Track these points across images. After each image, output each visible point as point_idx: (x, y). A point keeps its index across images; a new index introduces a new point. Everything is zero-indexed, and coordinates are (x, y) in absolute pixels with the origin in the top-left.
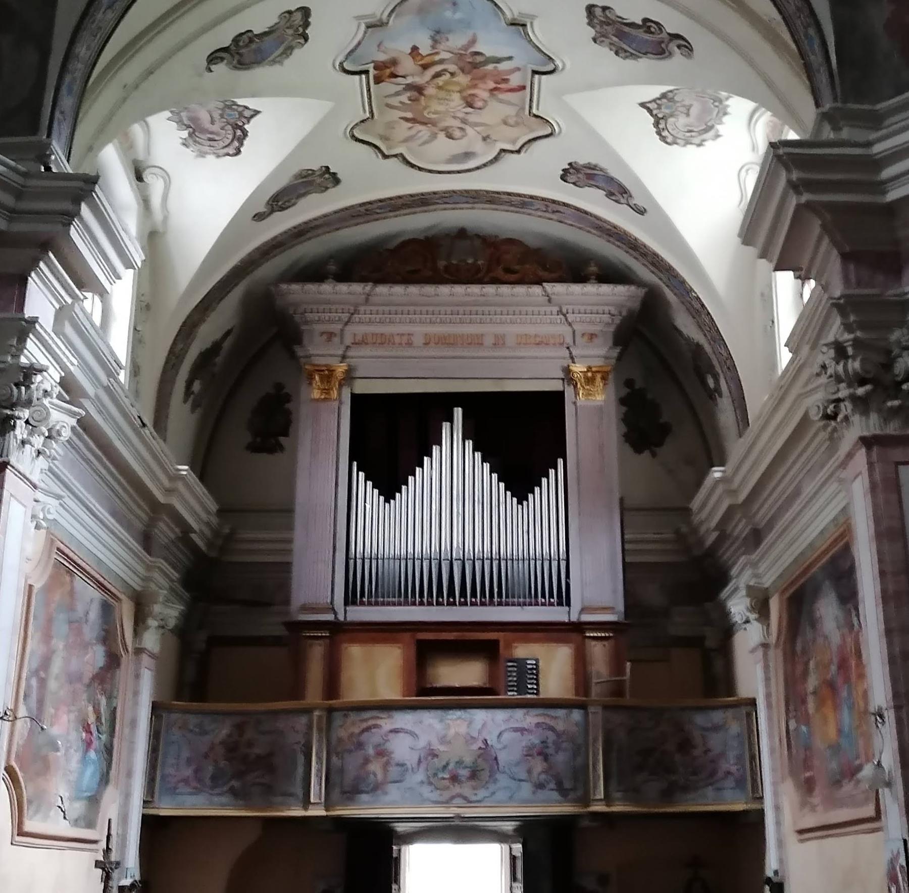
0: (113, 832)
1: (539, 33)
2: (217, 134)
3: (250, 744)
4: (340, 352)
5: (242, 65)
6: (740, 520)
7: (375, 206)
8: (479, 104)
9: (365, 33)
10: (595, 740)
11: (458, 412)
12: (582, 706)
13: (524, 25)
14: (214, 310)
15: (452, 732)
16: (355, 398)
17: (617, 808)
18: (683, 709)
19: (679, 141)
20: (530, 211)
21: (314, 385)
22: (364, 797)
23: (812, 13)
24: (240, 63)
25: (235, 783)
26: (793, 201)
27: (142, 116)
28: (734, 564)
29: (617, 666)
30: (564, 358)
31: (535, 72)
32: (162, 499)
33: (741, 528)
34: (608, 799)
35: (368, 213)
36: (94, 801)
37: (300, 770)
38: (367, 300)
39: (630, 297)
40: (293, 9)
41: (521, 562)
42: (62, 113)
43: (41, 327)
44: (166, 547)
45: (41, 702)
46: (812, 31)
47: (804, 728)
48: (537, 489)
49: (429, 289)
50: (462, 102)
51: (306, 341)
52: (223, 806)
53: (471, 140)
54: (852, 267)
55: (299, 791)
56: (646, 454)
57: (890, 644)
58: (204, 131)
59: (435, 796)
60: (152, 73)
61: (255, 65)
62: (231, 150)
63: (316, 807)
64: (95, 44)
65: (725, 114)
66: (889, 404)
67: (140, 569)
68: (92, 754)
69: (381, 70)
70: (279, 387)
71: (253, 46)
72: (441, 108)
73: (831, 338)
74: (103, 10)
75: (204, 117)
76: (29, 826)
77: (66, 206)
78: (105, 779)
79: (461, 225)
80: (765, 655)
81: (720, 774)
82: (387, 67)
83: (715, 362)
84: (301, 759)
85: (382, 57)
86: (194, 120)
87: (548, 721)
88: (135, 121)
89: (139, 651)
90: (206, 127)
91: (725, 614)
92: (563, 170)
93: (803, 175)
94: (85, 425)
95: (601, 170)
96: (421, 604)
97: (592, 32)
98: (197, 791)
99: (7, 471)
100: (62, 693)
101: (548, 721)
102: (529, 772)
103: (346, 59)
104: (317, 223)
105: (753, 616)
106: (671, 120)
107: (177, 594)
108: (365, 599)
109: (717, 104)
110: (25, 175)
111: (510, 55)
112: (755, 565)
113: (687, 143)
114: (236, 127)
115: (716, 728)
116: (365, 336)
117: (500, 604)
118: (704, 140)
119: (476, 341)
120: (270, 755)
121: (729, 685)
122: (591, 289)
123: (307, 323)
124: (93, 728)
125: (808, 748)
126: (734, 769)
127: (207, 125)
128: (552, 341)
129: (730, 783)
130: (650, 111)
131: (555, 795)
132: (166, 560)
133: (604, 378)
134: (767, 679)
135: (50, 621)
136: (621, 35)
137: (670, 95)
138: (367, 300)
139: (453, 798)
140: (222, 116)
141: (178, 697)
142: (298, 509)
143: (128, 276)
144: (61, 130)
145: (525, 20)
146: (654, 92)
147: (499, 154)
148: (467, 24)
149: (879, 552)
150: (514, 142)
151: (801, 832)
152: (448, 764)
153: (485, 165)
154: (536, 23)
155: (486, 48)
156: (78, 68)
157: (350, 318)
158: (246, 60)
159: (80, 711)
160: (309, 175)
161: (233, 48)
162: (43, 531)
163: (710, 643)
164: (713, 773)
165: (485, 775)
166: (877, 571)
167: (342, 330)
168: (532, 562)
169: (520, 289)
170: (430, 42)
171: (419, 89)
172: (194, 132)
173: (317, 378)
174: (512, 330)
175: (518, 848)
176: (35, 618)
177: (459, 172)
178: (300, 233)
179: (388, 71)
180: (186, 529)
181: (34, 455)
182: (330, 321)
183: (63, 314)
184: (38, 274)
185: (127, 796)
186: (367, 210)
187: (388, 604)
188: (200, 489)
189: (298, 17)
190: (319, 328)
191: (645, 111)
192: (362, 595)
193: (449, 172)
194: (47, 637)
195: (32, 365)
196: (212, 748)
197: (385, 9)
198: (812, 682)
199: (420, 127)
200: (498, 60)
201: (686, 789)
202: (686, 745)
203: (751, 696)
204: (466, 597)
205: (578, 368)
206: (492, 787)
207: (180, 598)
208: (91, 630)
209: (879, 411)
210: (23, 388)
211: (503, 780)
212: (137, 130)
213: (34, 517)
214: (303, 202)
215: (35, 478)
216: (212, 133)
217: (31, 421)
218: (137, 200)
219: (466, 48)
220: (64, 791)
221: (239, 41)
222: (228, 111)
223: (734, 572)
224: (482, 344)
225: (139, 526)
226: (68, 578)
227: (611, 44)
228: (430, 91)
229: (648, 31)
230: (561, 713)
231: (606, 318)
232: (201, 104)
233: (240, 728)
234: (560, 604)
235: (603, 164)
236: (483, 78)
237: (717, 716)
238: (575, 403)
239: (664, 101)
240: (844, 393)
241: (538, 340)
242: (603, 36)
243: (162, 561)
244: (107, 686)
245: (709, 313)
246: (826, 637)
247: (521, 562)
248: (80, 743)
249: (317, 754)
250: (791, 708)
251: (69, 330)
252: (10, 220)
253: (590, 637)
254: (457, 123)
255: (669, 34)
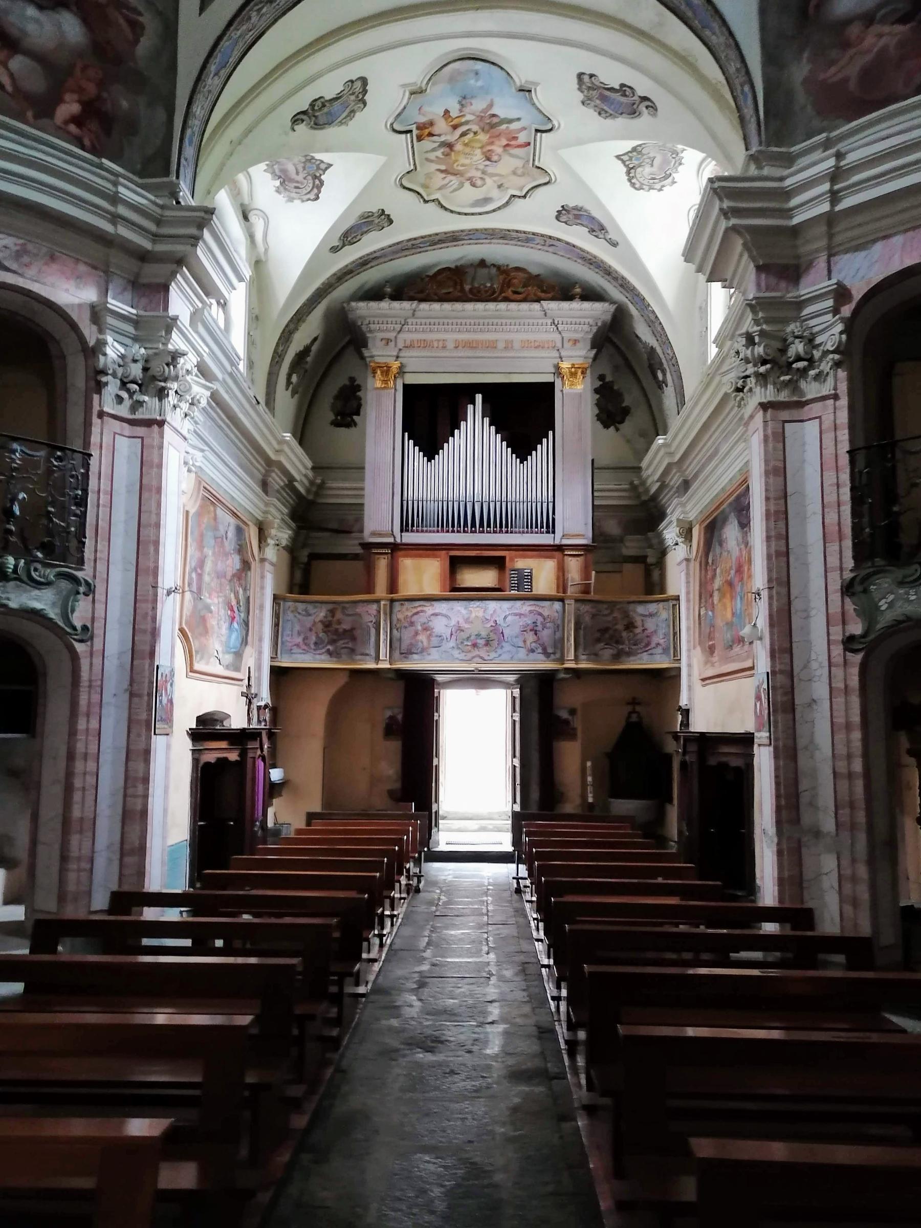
0: (252, 674)
1: (541, 97)
2: (302, 183)
3: (339, 622)
4: (395, 354)
5: (317, 125)
6: (675, 473)
7: (418, 241)
8: (495, 158)
9: (409, 98)
10: (569, 621)
11: (479, 398)
12: (562, 600)
13: (530, 91)
14: (304, 321)
15: (473, 615)
16: (406, 387)
17: (583, 665)
18: (629, 603)
19: (644, 187)
20: (533, 245)
21: (377, 377)
22: (415, 656)
23: (748, 73)
24: (316, 124)
25: (330, 647)
26: (723, 224)
27: (244, 168)
28: (669, 506)
29: (586, 575)
30: (555, 358)
31: (537, 131)
32: (273, 457)
33: (675, 480)
34: (576, 659)
35: (414, 247)
36: (238, 655)
37: (373, 639)
38: (413, 315)
39: (605, 312)
40: (354, 79)
41: (521, 504)
42: (186, 160)
43: (181, 322)
44: (278, 491)
45: (200, 589)
46: (747, 88)
47: (710, 613)
48: (534, 453)
49: (458, 306)
50: (482, 157)
51: (370, 345)
52: (323, 661)
53: (489, 188)
54: (763, 276)
55: (372, 652)
56: (612, 429)
57: (768, 547)
58: (291, 180)
59: (462, 656)
60: (251, 131)
61: (326, 126)
62: (312, 196)
63: (383, 662)
64: (208, 104)
65: (680, 164)
66: (782, 378)
67: (262, 506)
68: (235, 625)
69: (422, 130)
70: (352, 380)
71: (326, 110)
72: (467, 162)
73: (744, 330)
74: (212, 75)
75: (291, 168)
76: (197, 667)
77: (193, 231)
78: (245, 642)
79: (480, 258)
80: (687, 566)
81: (653, 645)
82: (426, 128)
83: (664, 361)
84: (373, 631)
85: (422, 119)
86: (284, 171)
87: (537, 609)
88: (241, 171)
89: (263, 560)
90: (292, 177)
91: (662, 541)
92: (558, 211)
93: (732, 204)
94: (215, 397)
95: (586, 211)
96: (453, 531)
97: (581, 96)
98: (306, 652)
99: (165, 426)
100: (213, 585)
101: (537, 609)
102: (525, 641)
103: (395, 120)
104: (375, 255)
105: (680, 540)
106: (639, 170)
107: (286, 523)
108: (415, 528)
109: (674, 156)
110: (162, 207)
111: (519, 117)
112: (683, 505)
113: (651, 188)
114: (315, 177)
115: (651, 615)
116: (412, 341)
117: (507, 532)
118: (663, 186)
119: (492, 345)
120: (353, 629)
121: (661, 587)
122: (576, 305)
123: (370, 331)
124: (235, 609)
125: (712, 626)
126: (662, 641)
127: (293, 175)
128: (546, 346)
129: (659, 650)
130: (623, 162)
131: (542, 657)
132: (279, 500)
133: (583, 373)
134: (688, 582)
135: (202, 536)
136: (603, 98)
137: (639, 149)
138: (413, 315)
139: (474, 657)
140: (304, 168)
141: (291, 593)
142: (367, 466)
143: (242, 288)
144: (186, 172)
145: (530, 86)
146: (626, 146)
147: (510, 199)
148: (485, 90)
149: (767, 484)
150: (521, 189)
151: (703, 680)
152: (470, 636)
153: (499, 208)
154: (538, 88)
155: (501, 110)
156: (195, 124)
157: (401, 328)
158: (321, 120)
159: (225, 596)
160: (369, 217)
161: (310, 111)
162: (193, 475)
163: (650, 560)
164: (648, 644)
165: (495, 643)
166: (764, 496)
167: (396, 337)
168: (529, 504)
169: (525, 306)
170: (458, 106)
171: (450, 146)
172: (284, 181)
173: (379, 372)
174: (518, 337)
175: (517, 692)
176: (192, 533)
177: (480, 214)
178: (364, 263)
179: (427, 131)
180: (291, 479)
181: (183, 416)
182: (387, 330)
183: (196, 316)
184: (176, 284)
185: (260, 653)
186: (413, 245)
187: (430, 532)
188: (299, 450)
189: (358, 84)
190: (380, 335)
191: (620, 162)
192: (413, 526)
193: (473, 214)
194: (201, 546)
195: (177, 350)
196: (315, 623)
197: (424, 78)
198: (718, 583)
199: (450, 177)
200: (510, 121)
201: (629, 654)
202: (630, 626)
203: (677, 594)
204: (483, 527)
205: (565, 365)
206: (499, 651)
207: (290, 527)
208: (230, 544)
209: (774, 384)
210: (172, 367)
211: (507, 647)
212: (241, 178)
213: (186, 463)
214: (365, 238)
215: (185, 432)
216: (297, 182)
217: (178, 391)
218: (245, 236)
219: (485, 111)
220: (218, 647)
221: (314, 105)
222: (308, 164)
223: (669, 511)
224: (496, 347)
225: (261, 477)
226: (212, 508)
227: (596, 106)
228: (459, 147)
229: (624, 95)
230: (547, 603)
231: (586, 328)
232: (288, 159)
233: (332, 612)
234: (548, 532)
235: (587, 207)
236: (498, 136)
237: (652, 607)
238: (562, 391)
239: (635, 154)
240: (751, 370)
241: (537, 344)
242: (589, 99)
243: (275, 499)
244: (243, 582)
245: (660, 323)
246: (729, 552)
247: (521, 504)
248: (227, 618)
249: (384, 628)
250: (703, 600)
251: (201, 329)
252: (154, 242)
253: (567, 555)
254: (479, 174)
255: (640, 97)
